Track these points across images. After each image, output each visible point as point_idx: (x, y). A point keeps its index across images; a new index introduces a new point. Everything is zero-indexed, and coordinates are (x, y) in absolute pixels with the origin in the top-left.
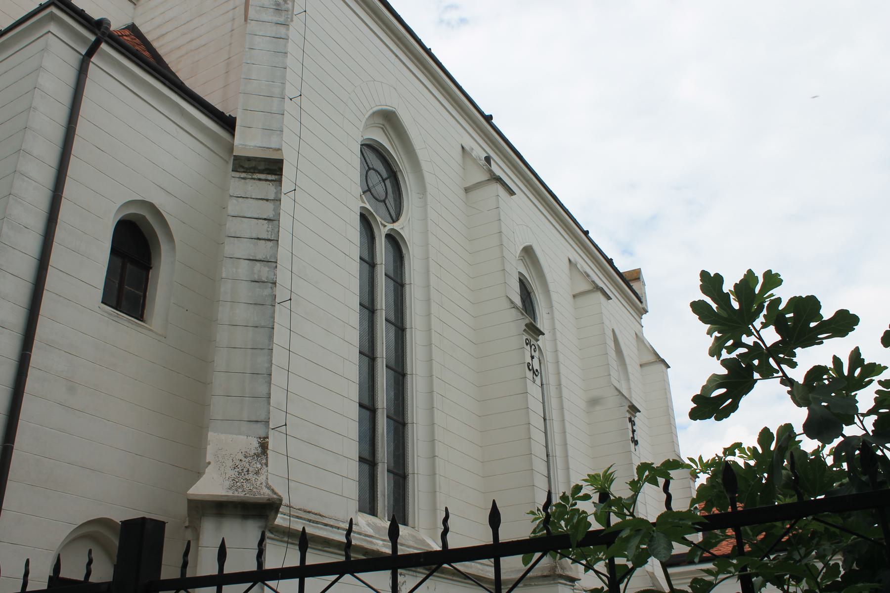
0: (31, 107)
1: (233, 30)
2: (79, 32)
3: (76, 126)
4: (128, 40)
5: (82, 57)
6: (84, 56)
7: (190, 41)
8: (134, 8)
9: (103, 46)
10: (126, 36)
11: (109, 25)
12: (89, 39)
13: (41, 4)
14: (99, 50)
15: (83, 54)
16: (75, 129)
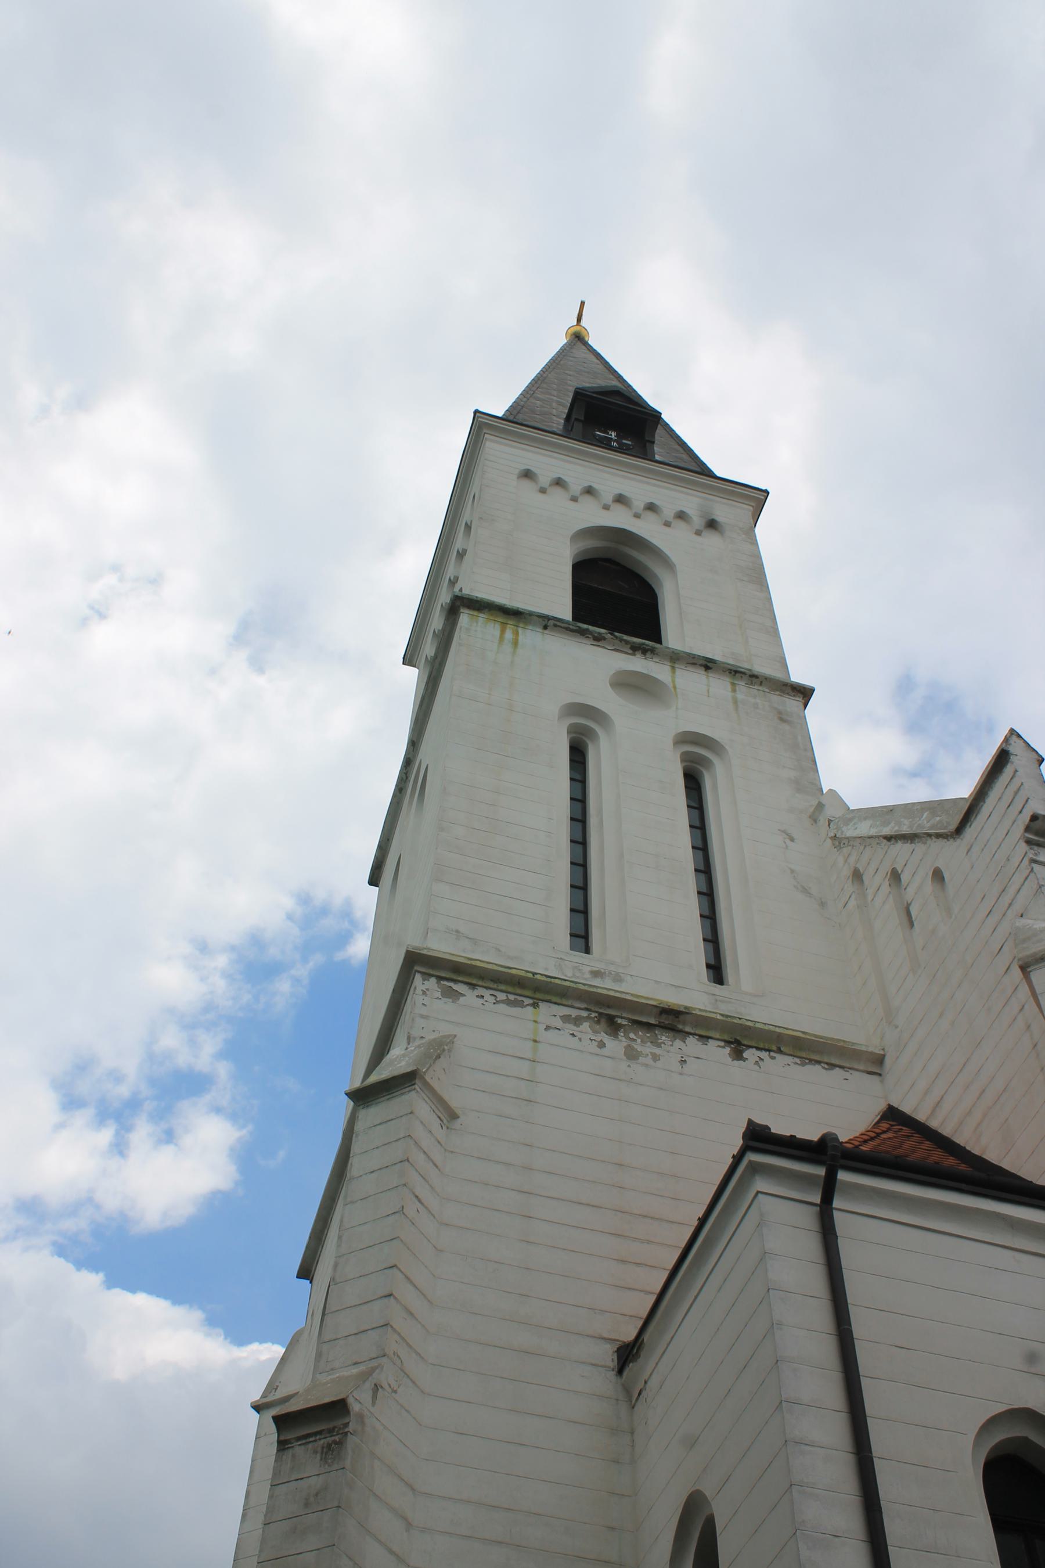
0: (773, 1324)
1: (1035, 1045)
2: (799, 1171)
3: (850, 1325)
4: (889, 1138)
5: (818, 1208)
6: (820, 1206)
7: (981, 1094)
8: (882, 1082)
9: (843, 1176)
10: (884, 1132)
11: (836, 1139)
12: (818, 1176)
13: (699, 1219)
14: (838, 1185)
15: (819, 1202)
16: (852, 1331)
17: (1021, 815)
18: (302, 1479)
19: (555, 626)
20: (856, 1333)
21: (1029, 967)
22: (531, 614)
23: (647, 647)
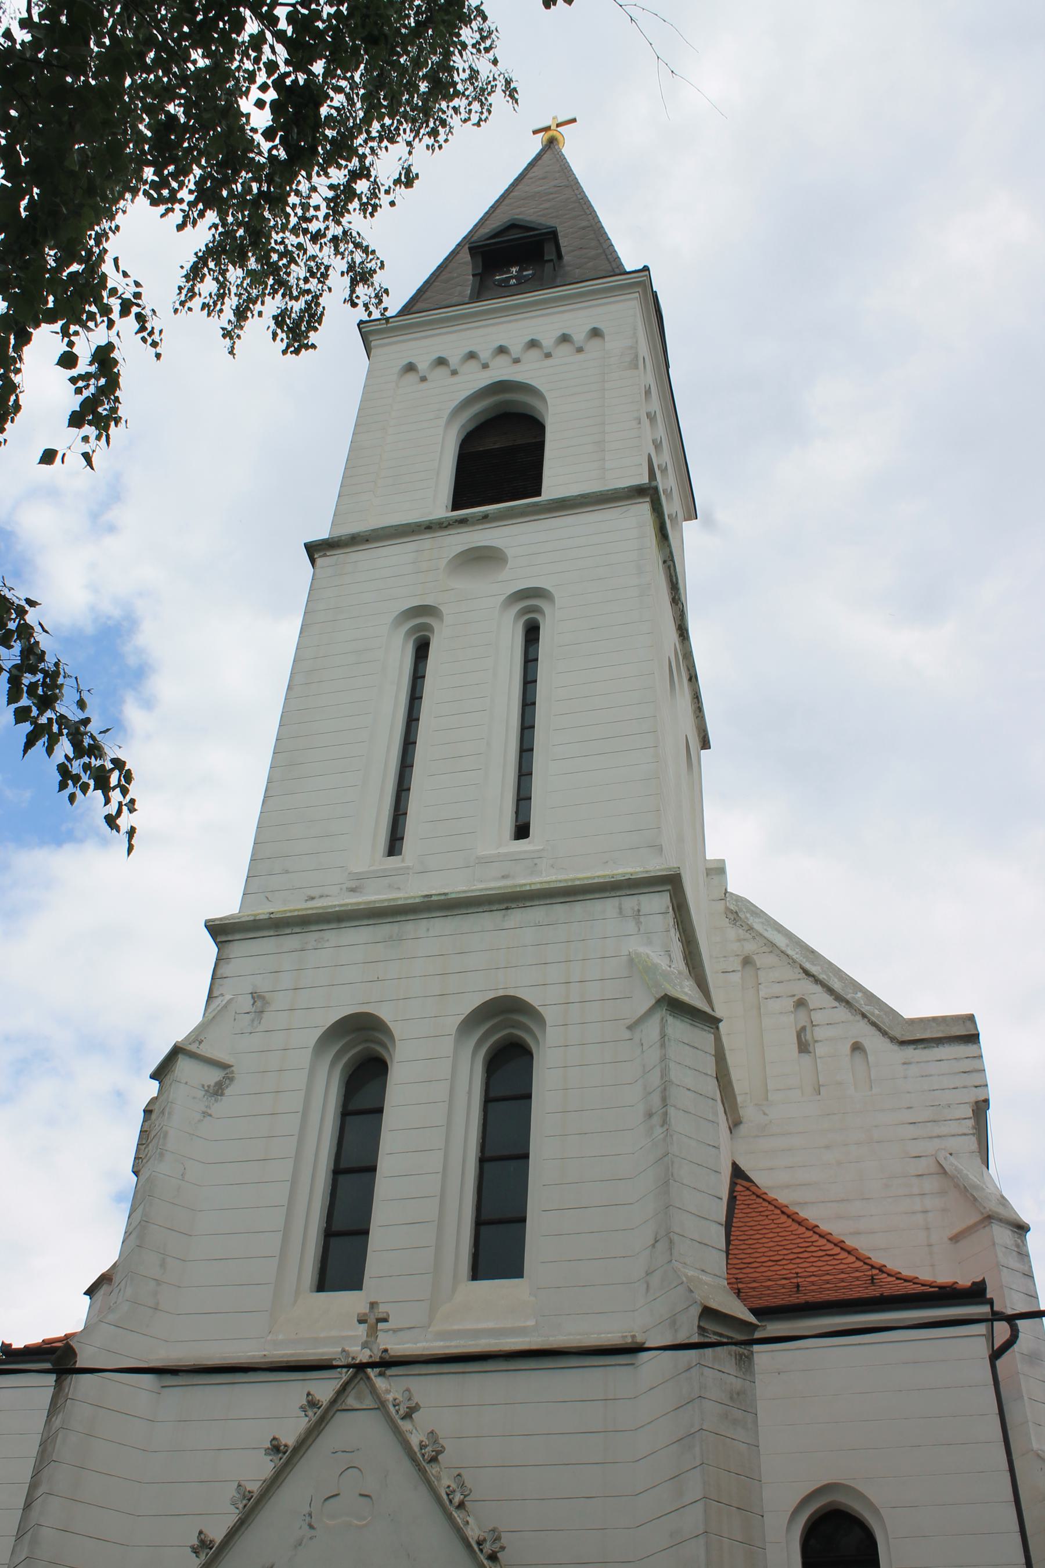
17: (974, 1089)
18: (723, 1372)
19: (669, 567)
20: (1009, 1474)
21: (993, 1219)
22: (669, 546)
23: (685, 635)
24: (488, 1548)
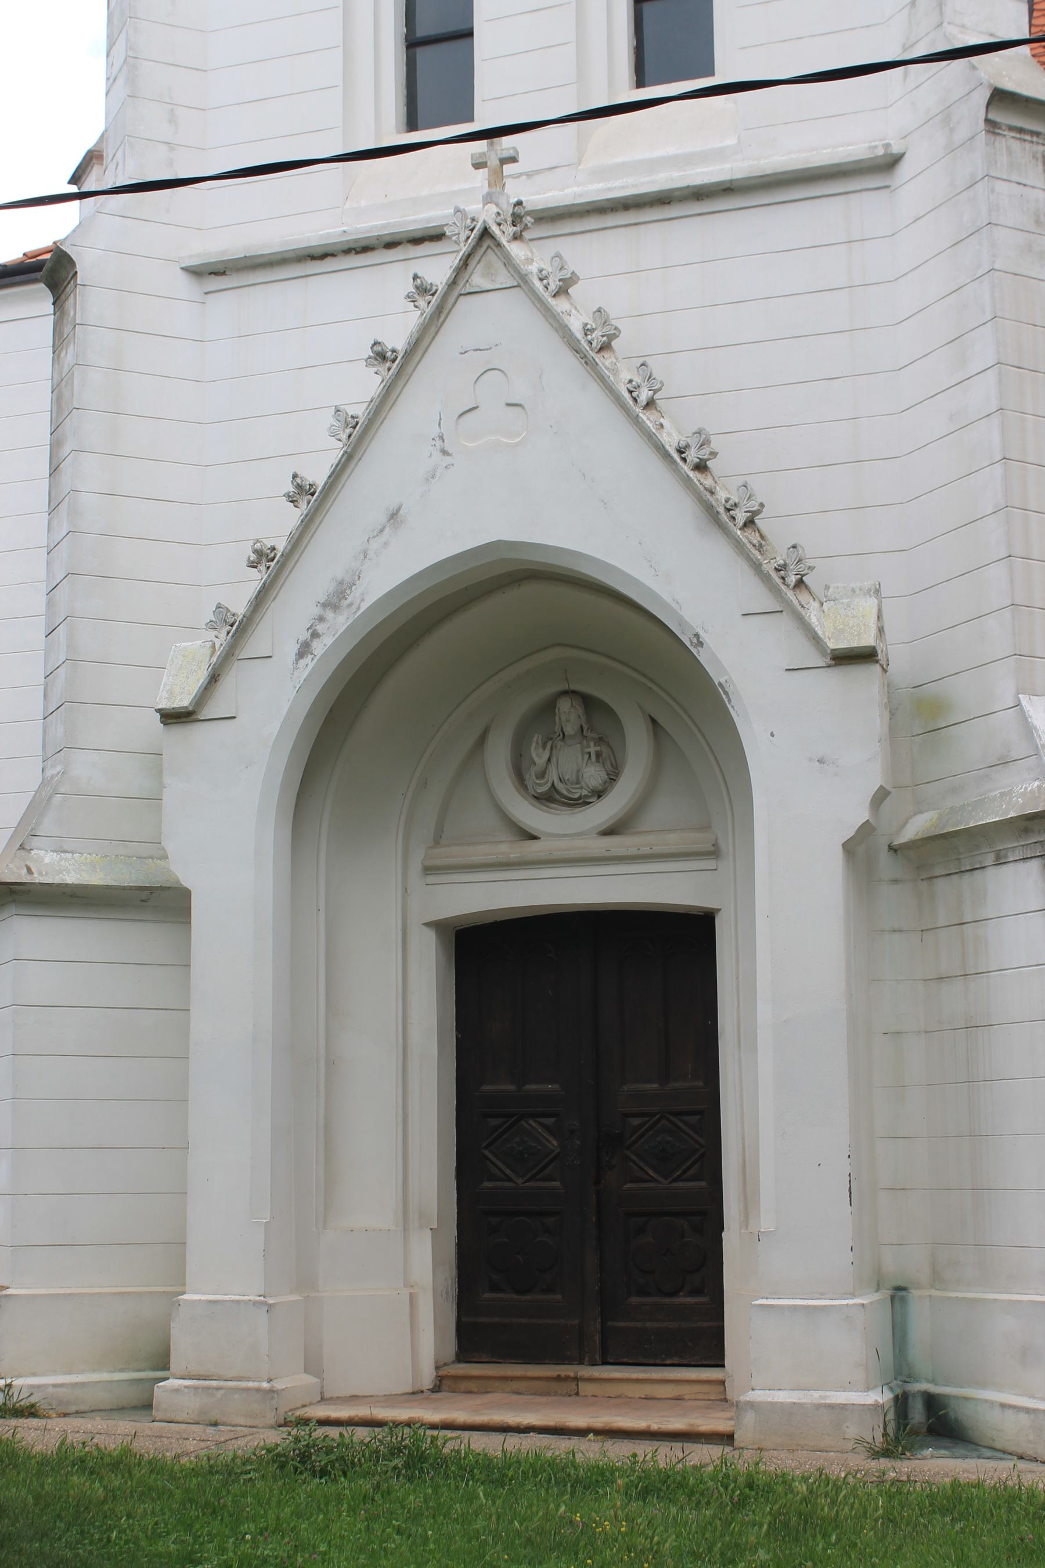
24: (692, 456)
